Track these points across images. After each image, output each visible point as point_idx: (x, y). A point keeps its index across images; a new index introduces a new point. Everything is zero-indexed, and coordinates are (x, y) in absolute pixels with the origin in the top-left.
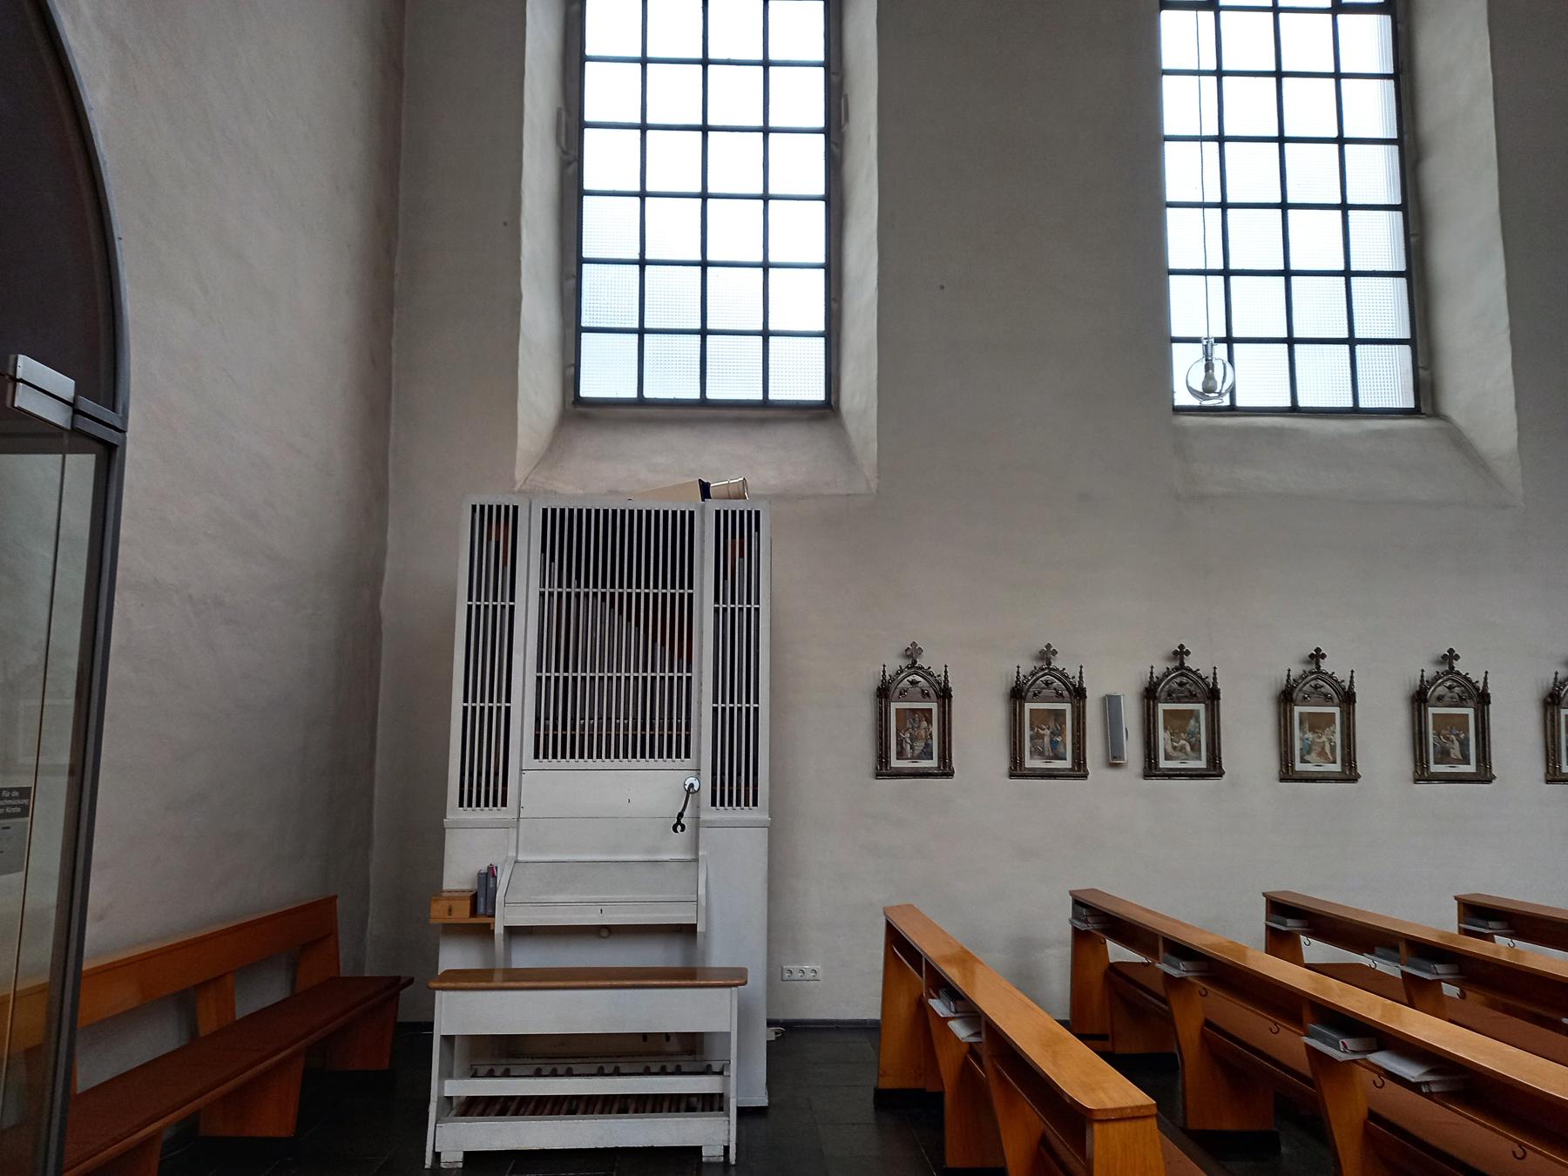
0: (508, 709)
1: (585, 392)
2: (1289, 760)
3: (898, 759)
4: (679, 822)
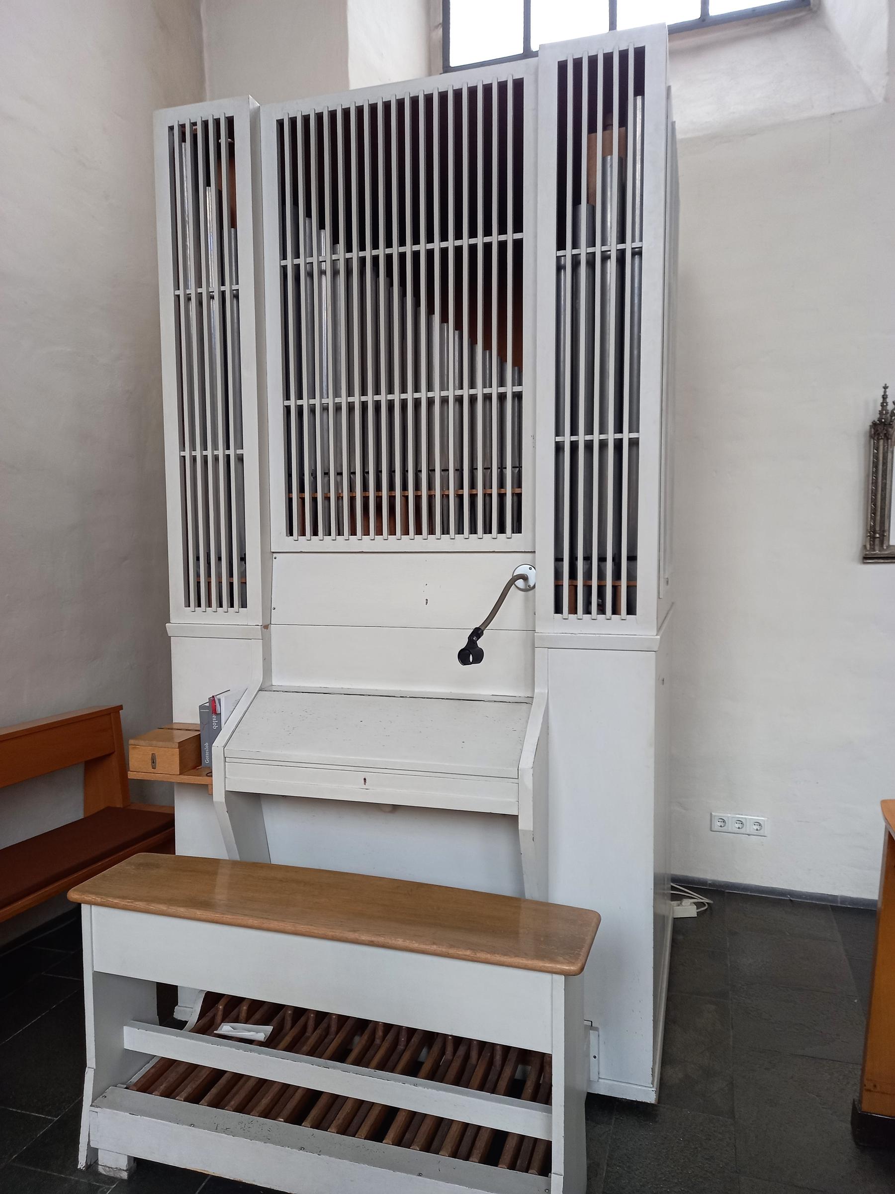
2: (878, 529)
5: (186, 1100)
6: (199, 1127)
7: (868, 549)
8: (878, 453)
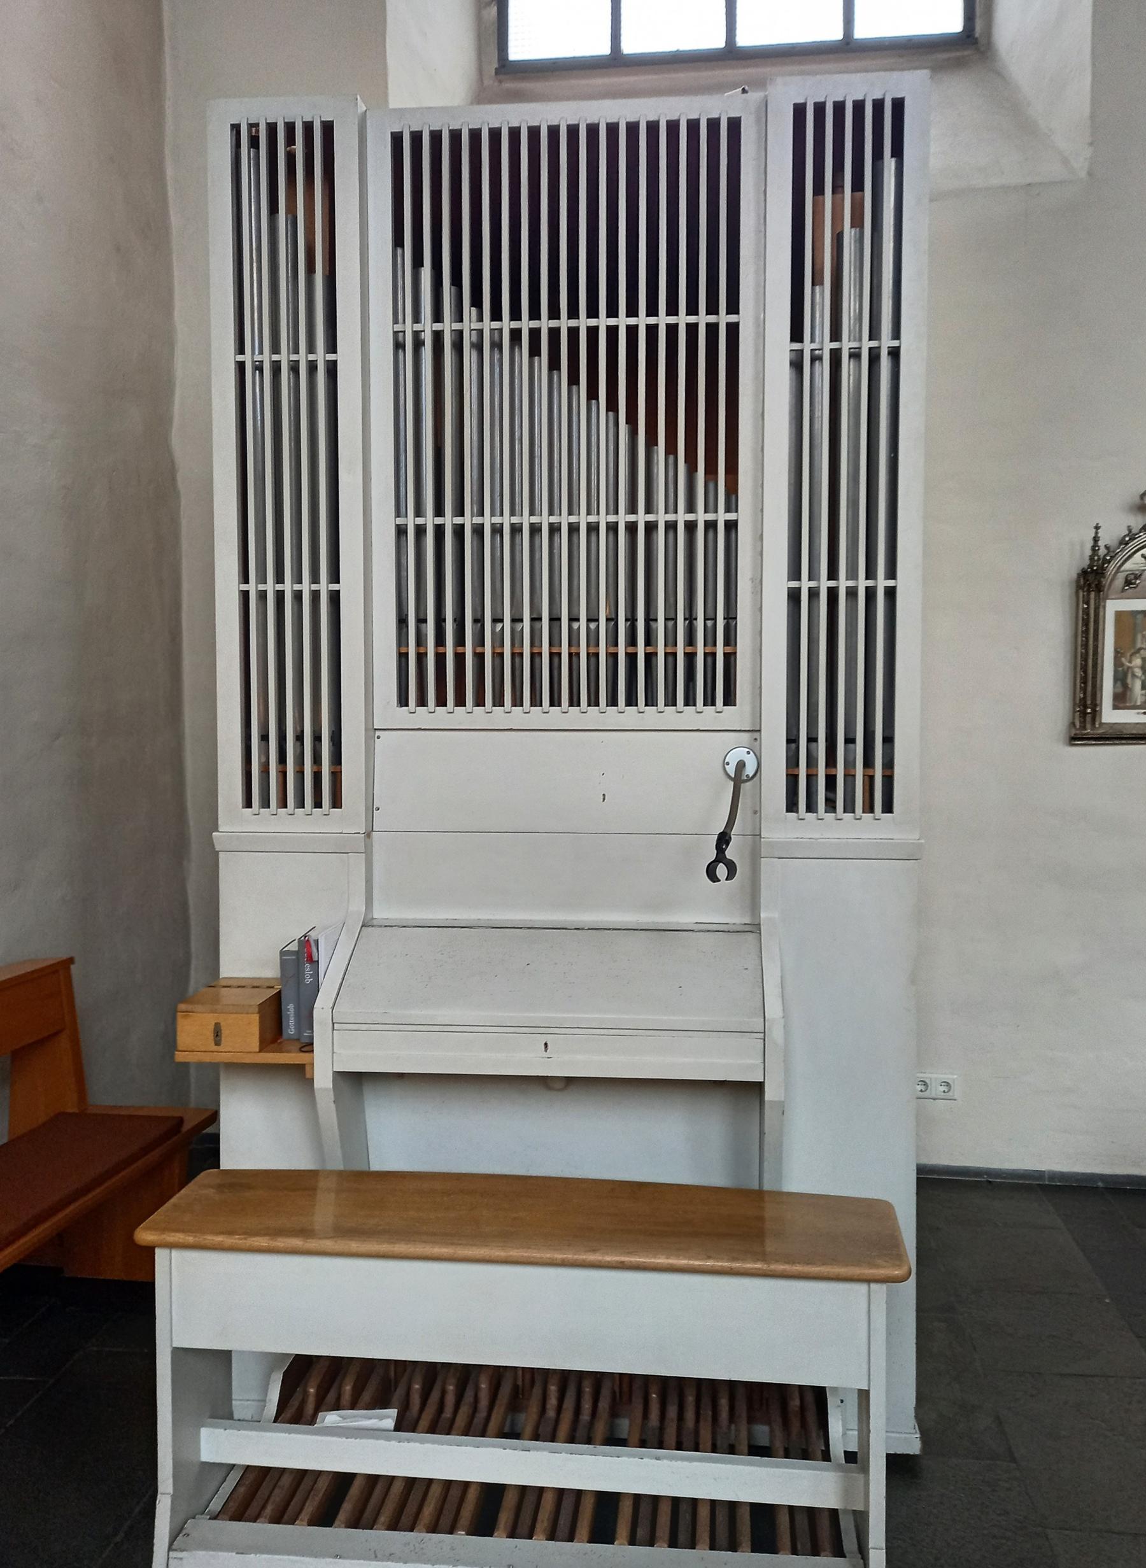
0: (335, 597)
1: (516, 53)
2: (1089, 702)
3: (1116, 707)
4: (720, 857)
5: (311, 1523)
6: (345, 1558)
7: (1078, 727)
8: (1088, 608)
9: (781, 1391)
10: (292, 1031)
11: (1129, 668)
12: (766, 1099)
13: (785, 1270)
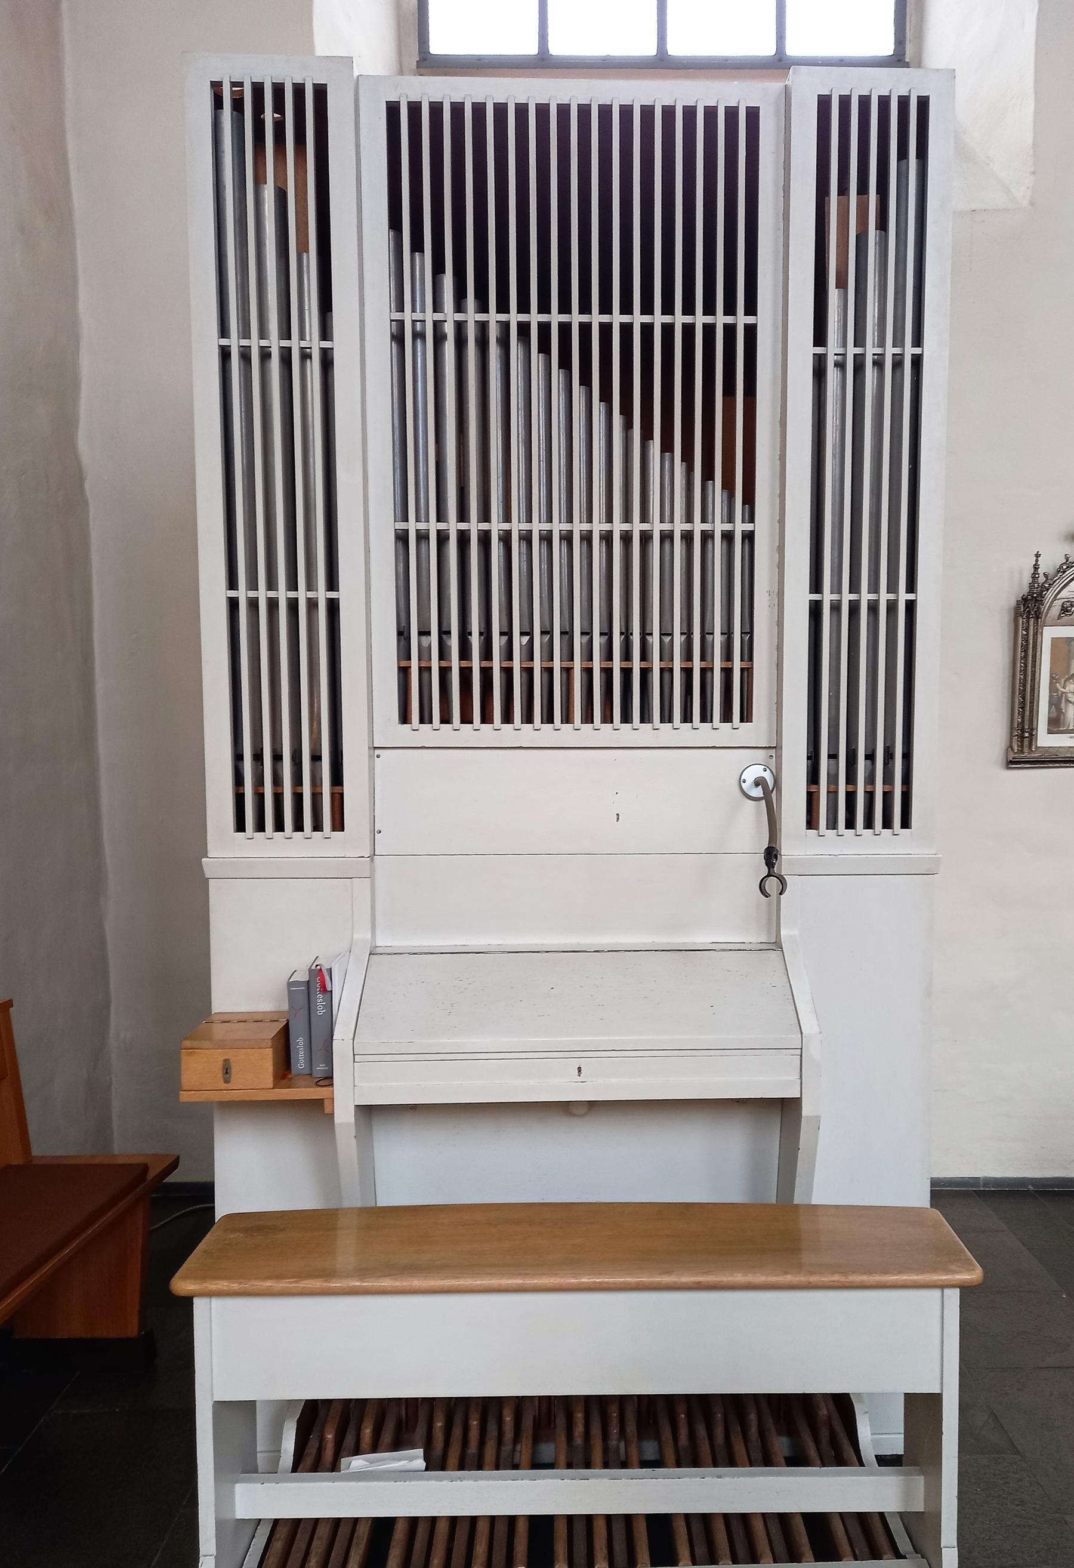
0: (333, 607)
2: (1026, 727)
3: (1050, 732)
8: (1027, 634)
9: (805, 1402)
10: (302, 1066)
11: (1063, 693)
12: (803, 1115)
13: (862, 1281)
